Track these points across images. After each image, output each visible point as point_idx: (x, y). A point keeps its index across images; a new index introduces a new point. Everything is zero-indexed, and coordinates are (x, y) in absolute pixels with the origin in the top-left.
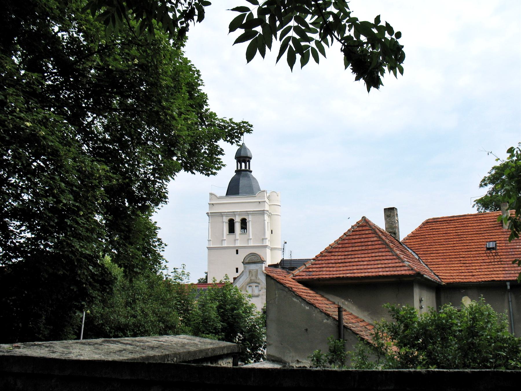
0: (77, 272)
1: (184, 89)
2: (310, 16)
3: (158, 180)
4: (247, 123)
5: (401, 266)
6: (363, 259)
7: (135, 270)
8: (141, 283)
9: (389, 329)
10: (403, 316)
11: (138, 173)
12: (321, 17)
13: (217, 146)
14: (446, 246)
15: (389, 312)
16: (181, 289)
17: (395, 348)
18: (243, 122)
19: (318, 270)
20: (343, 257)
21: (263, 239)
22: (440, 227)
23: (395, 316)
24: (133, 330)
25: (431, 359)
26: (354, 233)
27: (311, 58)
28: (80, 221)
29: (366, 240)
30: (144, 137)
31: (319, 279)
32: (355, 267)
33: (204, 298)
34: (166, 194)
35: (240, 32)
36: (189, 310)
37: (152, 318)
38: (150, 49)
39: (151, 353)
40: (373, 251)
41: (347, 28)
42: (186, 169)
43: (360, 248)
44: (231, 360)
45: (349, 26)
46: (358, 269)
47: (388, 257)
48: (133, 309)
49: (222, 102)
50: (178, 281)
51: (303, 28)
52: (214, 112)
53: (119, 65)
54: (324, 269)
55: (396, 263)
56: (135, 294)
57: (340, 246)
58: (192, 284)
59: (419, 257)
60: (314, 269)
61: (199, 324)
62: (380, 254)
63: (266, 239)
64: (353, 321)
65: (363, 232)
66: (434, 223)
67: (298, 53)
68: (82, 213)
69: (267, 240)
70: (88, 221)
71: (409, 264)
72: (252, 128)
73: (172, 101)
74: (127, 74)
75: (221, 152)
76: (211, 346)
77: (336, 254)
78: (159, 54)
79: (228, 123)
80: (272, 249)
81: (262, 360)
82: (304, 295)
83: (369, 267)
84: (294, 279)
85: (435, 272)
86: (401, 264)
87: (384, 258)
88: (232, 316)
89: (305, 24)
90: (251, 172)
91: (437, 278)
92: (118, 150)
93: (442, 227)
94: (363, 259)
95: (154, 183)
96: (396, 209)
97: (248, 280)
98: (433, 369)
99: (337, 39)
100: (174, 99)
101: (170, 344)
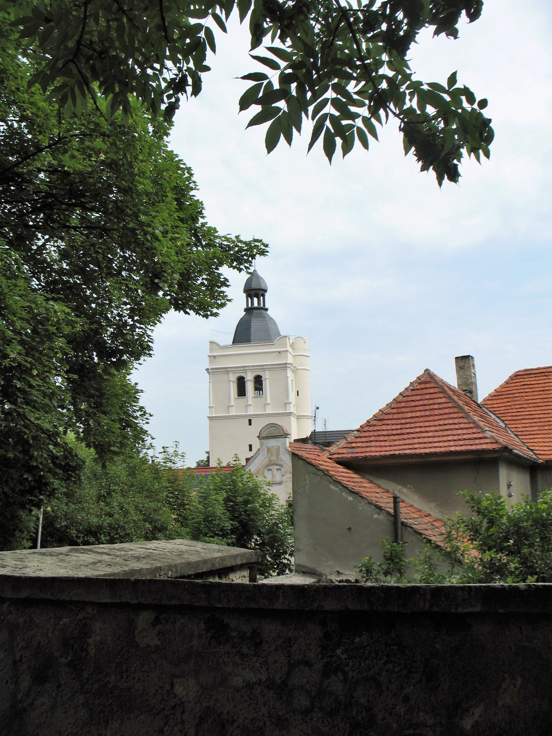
0: (33, 454)
1: (171, 195)
2: (353, 83)
3: (138, 325)
4: (260, 241)
5: (480, 438)
6: (427, 429)
7: (112, 448)
8: (118, 468)
9: (466, 526)
10: (487, 508)
11: (109, 316)
12: (370, 83)
13: (220, 274)
14: (544, 408)
15: (467, 502)
16: (174, 477)
17: (475, 553)
18: (255, 241)
19: (364, 445)
20: (399, 427)
21: (286, 404)
22: (535, 382)
23: (476, 508)
24: (109, 534)
25: (527, 567)
26: (414, 393)
27: (357, 142)
28: (34, 383)
29: (431, 402)
30: (116, 265)
31: (365, 458)
32: (415, 441)
33: (205, 487)
34: (149, 343)
35: (255, 109)
36: (185, 505)
37: (135, 516)
38: (120, 140)
39: (137, 565)
40: (440, 417)
41: (408, 97)
42: (178, 308)
43: (423, 413)
44: (246, 573)
45: (410, 94)
46: (420, 443)
47: (462, 426)
48: (108, 504)
49: (223, 214)
50: (169, 464)
51: (344, 100)
52: (213, 226)
53: (78, 165)
54: (373, 444)
55: (474, 433)
56: (110, 484)
57: (394, 411)
58: (189, 469)
59: (506, 424)
60: (359, 445)
61: (199, 523)
62: (451, 421)
63: (290, 403)
64: (415, 516)
65: (426, 391)
66: (526, 377)
67: (338, 137)
68: (35, 372)
69: (292, 405)
70: (45, 382)
71: (493, 435)
72: (267, 249)
73: (154, 214)
74: (90, 177)
75: (225, 283)
76: (219, 555)
77: (389, 422)
78: (134, 147)
79: (233, 242)
80: (299, 417)
81: (287, 571)
82: (345, 481)
83: (436, 439)
84: (330, 458)
85: (528, 445)
86: (480, 435)
87: (457, 426)
88: (245, 511)
89: (347, 95)
90: (267, 310)
91: (532, 453)
92: (80, 285)
93: (538, 382)
94: (427, 429)
95: (133, 327)
96: (472, 357)
97: (266, 461)
98: (531, 581)
99: (394, 114)
100: (157, 212)
101: (161, 553)
